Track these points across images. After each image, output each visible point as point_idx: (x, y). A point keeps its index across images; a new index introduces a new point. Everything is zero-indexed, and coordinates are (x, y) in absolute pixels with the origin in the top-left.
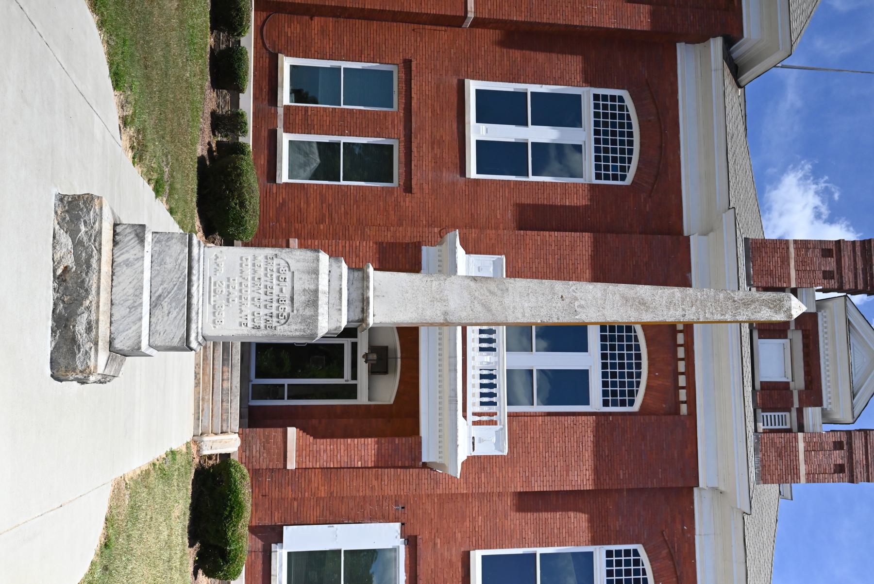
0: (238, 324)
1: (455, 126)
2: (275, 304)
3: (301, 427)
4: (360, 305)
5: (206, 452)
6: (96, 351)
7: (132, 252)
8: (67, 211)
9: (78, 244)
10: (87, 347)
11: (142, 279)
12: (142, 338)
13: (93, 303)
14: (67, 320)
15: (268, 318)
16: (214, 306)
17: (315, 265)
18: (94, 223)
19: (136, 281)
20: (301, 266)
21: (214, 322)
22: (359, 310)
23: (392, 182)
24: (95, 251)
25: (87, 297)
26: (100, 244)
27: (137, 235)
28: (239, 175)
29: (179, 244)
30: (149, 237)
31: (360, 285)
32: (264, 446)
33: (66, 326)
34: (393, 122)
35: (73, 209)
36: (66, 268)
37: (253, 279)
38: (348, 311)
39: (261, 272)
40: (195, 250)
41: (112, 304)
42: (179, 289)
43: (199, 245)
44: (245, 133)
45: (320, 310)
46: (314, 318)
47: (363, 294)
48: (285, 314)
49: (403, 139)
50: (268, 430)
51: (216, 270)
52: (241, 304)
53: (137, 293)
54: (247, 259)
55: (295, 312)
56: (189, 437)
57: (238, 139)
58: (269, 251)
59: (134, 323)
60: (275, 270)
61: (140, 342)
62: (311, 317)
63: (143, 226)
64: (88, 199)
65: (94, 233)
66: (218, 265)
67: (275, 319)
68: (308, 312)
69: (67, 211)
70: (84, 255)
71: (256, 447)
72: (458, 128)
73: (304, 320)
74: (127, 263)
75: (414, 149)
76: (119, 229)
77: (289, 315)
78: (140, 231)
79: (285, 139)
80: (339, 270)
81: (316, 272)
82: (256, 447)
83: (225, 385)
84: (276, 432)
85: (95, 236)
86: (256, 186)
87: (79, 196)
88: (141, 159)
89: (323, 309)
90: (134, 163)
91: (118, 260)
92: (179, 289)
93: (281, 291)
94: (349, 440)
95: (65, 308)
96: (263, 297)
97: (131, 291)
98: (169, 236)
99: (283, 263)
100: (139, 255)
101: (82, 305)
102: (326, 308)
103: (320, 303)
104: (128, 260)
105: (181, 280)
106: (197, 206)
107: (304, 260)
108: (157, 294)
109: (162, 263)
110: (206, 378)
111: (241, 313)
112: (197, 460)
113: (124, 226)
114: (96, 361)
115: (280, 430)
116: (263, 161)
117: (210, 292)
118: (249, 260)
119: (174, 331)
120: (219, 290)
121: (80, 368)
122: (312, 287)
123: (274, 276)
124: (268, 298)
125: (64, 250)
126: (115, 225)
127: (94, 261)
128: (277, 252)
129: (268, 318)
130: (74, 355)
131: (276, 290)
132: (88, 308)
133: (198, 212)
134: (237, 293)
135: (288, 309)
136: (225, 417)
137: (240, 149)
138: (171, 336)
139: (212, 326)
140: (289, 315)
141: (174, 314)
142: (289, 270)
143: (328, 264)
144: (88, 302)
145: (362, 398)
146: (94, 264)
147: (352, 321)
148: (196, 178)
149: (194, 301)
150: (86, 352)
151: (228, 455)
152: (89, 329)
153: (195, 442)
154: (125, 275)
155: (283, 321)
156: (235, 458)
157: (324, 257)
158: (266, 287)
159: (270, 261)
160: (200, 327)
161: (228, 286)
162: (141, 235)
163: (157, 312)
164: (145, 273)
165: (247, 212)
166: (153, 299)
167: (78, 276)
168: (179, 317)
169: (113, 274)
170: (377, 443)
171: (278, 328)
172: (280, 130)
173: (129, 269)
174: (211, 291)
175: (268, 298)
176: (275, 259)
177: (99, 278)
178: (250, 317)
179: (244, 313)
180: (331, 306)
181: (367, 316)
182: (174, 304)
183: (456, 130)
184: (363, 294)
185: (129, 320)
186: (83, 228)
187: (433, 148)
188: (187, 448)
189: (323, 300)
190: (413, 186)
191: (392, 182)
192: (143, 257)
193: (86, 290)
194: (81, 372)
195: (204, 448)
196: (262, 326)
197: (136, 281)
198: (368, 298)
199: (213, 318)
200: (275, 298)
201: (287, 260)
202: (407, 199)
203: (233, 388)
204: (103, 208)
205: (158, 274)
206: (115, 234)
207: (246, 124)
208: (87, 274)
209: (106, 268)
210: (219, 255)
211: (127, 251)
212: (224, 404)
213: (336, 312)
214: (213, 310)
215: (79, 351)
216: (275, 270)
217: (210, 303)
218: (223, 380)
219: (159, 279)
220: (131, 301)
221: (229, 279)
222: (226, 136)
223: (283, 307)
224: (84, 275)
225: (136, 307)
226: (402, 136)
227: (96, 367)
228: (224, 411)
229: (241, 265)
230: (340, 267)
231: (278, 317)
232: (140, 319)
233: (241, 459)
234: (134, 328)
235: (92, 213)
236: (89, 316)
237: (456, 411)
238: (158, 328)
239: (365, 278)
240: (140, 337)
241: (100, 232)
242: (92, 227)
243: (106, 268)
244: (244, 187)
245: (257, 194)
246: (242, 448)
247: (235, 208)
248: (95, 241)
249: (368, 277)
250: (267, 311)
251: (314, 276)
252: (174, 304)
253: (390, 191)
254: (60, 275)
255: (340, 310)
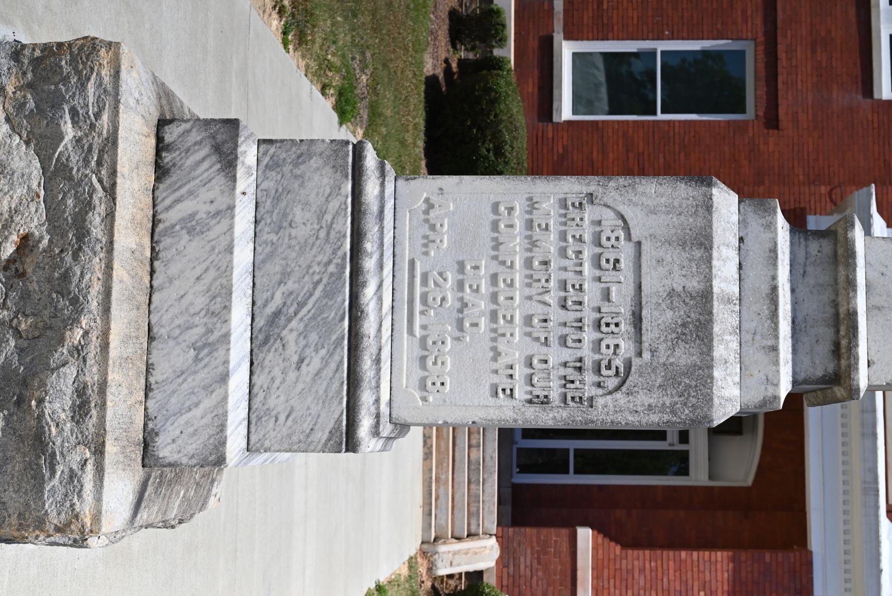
0: (486, 390)
1: (852, 12)
2: (589, 335)
3: (598, 527)
4: (826, 333)
5: (443, 571)
6: (100, 471)
7: (205, 194)
8: (30, 86)
9: (56, 173)
10: (74, 459)
11: (229, 268)
12: (229, 431)
13: (93, 336)
14: (25, 383)
15: (571, 373)
16: (424, 339)
17: (700, 222)
18: (98, 116)
19: (212, 273)
20: (661, 224)
21: (423, 387)
22: (824, 349)
23: (743, 111)
24: (100, 193)
25: (77, 321)
26: (113, 173)
27: (217, 149)
28: (494, 102)
29: (328, 170)
30: (248, 154)
31: (825, 278)
32: (539, 559)
33: (19, 402)
34: (744, 12)
35: (46, 80)
36: (25, 239)
37: (528, 263)
38: (795, 351)
39: (550, 244)
40: (371, 188)
41: (151, 338)
42: (329, 294)
43: (383, 174)
44: (502, 41)
45: (719, 351)
46: (701, 376)
47: (835, 305)
48: (618, 362)
49: (761, 39)
50: (544, 531)
51: (428, 242)
52: (496, 335)
53: (216, 307)
54: (510, 210)
55: (647, 355)
56: (412, 547)
57: (491, 52)
58: (571, 186)
59: (208, 389)
60: (587, 237)
61: (223, 443)
62: (690, 371)
63: (233, 124)
64: (85, 51)
65: (97, 142)
66: (433, 227)
67: (589, 377)
68: (684, 357)
69: (30, 86)
70: (70, 202)
71: (526, 560)
72: (858, 16)
73: (672, 378)
74: (192, 226)
75: (782, 55)
76: (171, 134)
77: (628, 365)
78: (224, 136)
79: (567, 51)
80: (767, 235)
81: (702, 242)
82: (526, 560)
83: (473, 456)
84: (556, 536)
85: (101, 152)
86: (521, 120)
87: (60, 45)
88: (301, 40)
89: (725, 347)
90: (285, 44)
91: (169, 217)
92: (329, 294)
93: (606, 296)
94: (683, 554)
95: (21, 351)
96: (556, 315)
97: (200, 302)
98: (303, 149)
99: (609, 218)
100: (222, 203)
101: (61, 341)
102: (735, 345)
103: (716, 329)
104: (192, 216)
105: (332, 268)
106: (427, 155)
107: (670, 209)
108: (270, 309)
109: (283, 224)
110: (443, 444)
111: (495, 359)
112: (428, 584)
113: (185, 126)
114: (98, 499)
115: (564, 532)
116: (531, 87)
117: (411, 302)
118: (517, 212)
119: (314, 411)
120: (435, 295)
121: (54, 519)
122: (694, 284)
123: (586, 255)
124: (571, 316)
125: (20, 191)
126: (162, 123)
127: (97, 220)
128: (592, 188)
129: (571, 373)
130: (39, 482)
131: (591, 294)
132: (78, 351)
133: (427, 166)
134: (483, 305)
135: (626, 348)
136: (473, 509)
137: (498, 64)
138: (307, 427)
139: (417, 395)
140: (628, 365)
141: (316, 363)
142: (629, 237)
143: (735, 218)
144: (78, 333)
145: (699, 475)
146: (97, 230)
147: (805, 382)
148: (422, 106)
149: (369, 327)
150: (72, 475)
151: (479, 574)
152: (80, 410)
153: (424, 554)
154: (185, 256)
155: (612, 383)
156: (490, 580)
157: (725, 201)
158: (563, 285)
159: (573, 213)
160: (385, 397)
161: (460, 285)
162: (226, 148)
163: (270, 358)
164: (236, 250)
165: (506, 163)
166: (260, 322)
167: (53, 259)
168: (328, 372)
169: (154, 256)
170: (733, 559)
171: (600, 402)
172: (558, 36)
173: (197, 243)
174: (414, 300)
175: (571, 316)
176: (588, 208)
177: (109, 267)
178: (520, 372)
179: (503, 361)
180: (747, 337)
181: (853, 367)
182: (313, 337)
183: (854, 20)
184: (835, 305)
185: (193, 382)
186: (69, 131)
187: (814, 52)
188: (410, 567)
189: (724, 319)
190: (782, 116)
191: (743, 111)
192: (231, 208)
193: (75, 301)
194: (58, 530)
195: (439, 564)
196: (555, 395)
197: (212, 273)
198: (852, 315)
199: (419, 373)
200: (589, 316)
201: (621, 208)
202: (771, 140)
203: (488, 458)
204: (123, 75)
205: (271, 256)
206: (161, 146)
207: (504, 26)
208: (75, 257)
209: (130, 238)
210: (434, 199)
211: (191, 193)
212: (473, 486)
213: (760, 356)
214: (418, 352)
215: (53, 472)
216: (587, 237)
217: (411, 332)
218: (470, 447)
219: (274, 268)
220: (200, 330)
221: (461, 266)
222: (473, 49)
223: (611, 341)
224: (68, 259)
225: (213, 343)
226: (760, 34)
227: (97, 517)
228: (473, 499)
229: (495, 226)
230: (771, 226)
231: (598, 370)
232: (224, 378)
233: (500, 578)
234: (208, 403)
235: (91, 87)
236: (80, 372)
237: (877, 508)
238: (272, 402)
239: (843, 256)
240: (222, 427)
241: (112, 141)
242: (92, 126)
243: (130, 238)
244: (501, 121)
245: (523, 133)
246: (502, 562)
247: (486, 158)
248: (99, 163)
249: (851, 254)
250: (567, 355)
251: (698, 253)
252: (313, 337)
253: (741, 127)
254: (11, 261)
255: (775, 349)
